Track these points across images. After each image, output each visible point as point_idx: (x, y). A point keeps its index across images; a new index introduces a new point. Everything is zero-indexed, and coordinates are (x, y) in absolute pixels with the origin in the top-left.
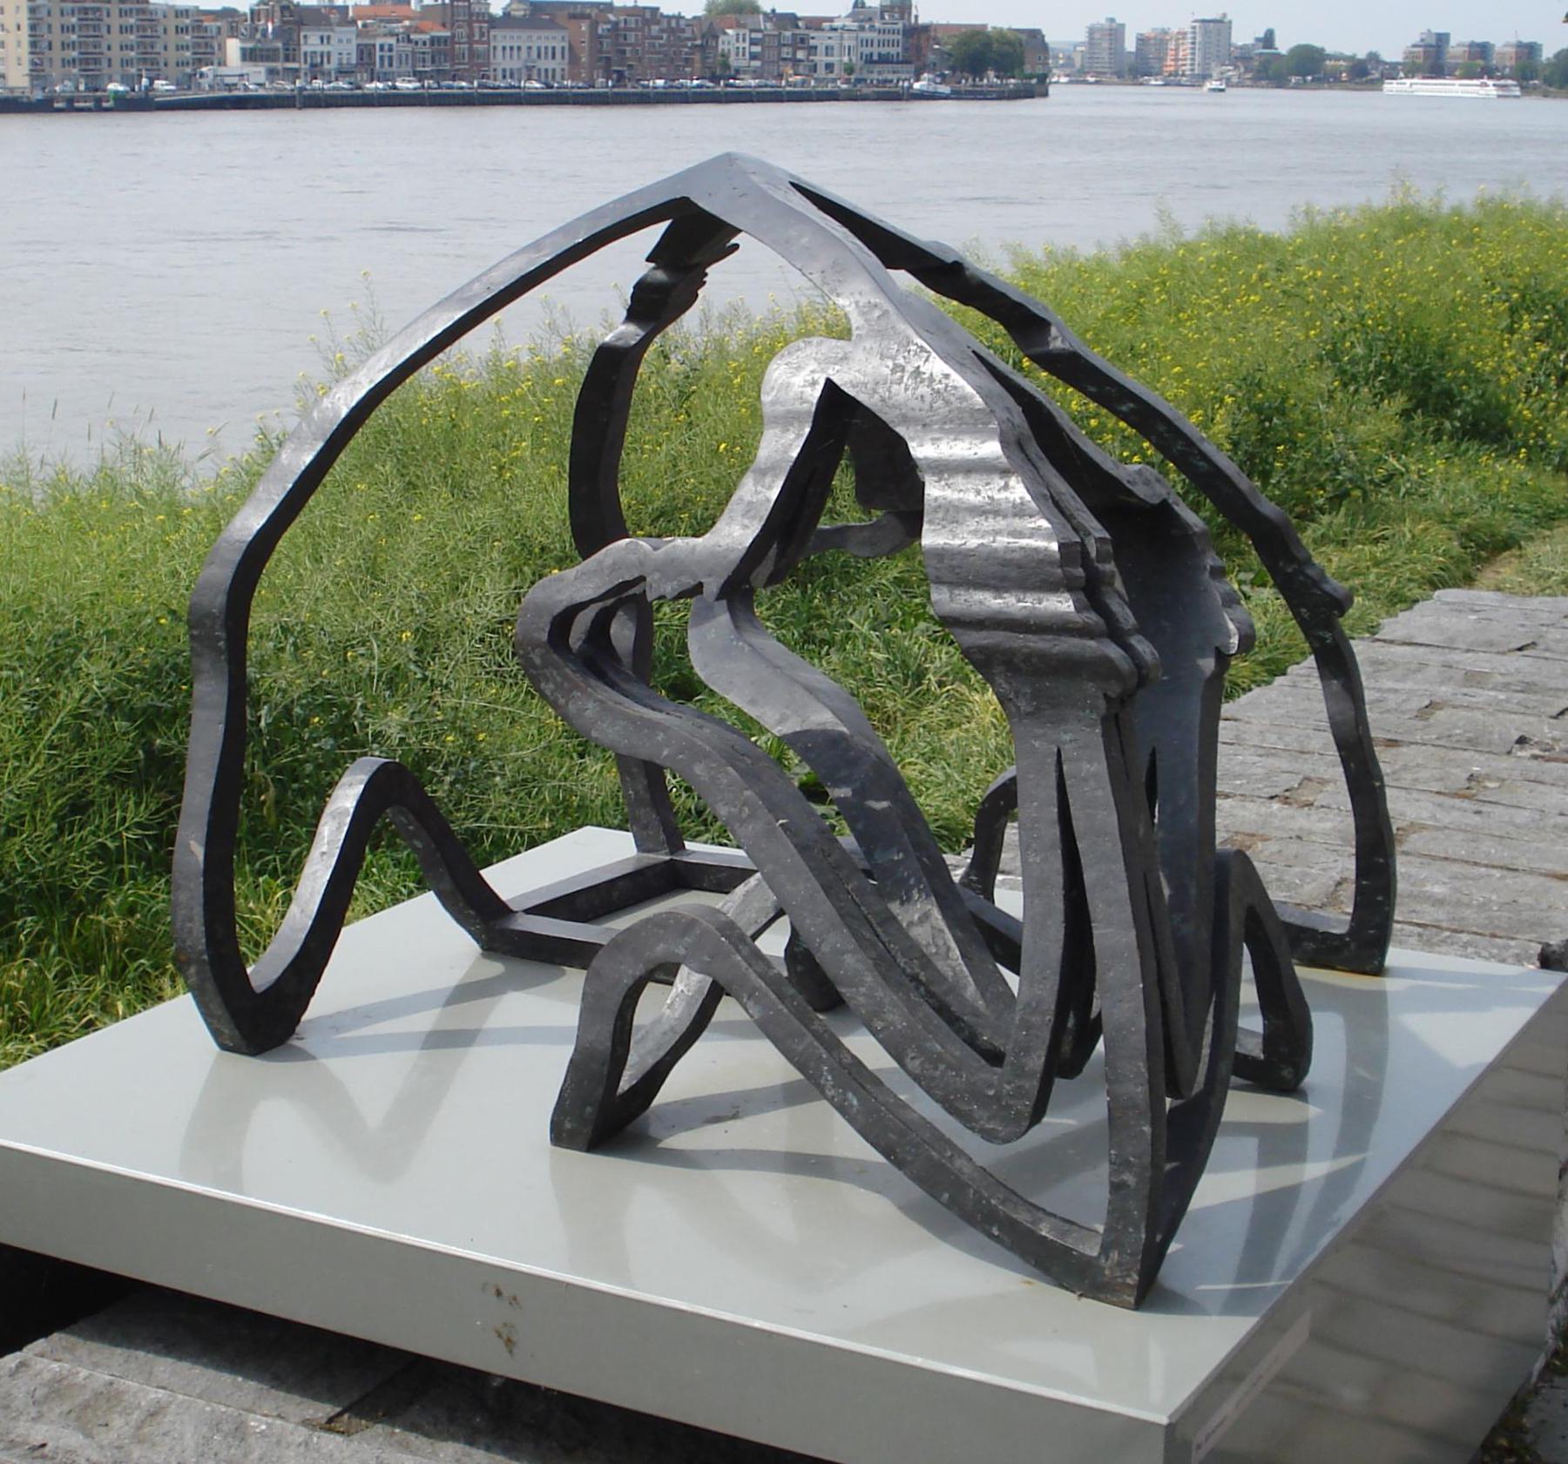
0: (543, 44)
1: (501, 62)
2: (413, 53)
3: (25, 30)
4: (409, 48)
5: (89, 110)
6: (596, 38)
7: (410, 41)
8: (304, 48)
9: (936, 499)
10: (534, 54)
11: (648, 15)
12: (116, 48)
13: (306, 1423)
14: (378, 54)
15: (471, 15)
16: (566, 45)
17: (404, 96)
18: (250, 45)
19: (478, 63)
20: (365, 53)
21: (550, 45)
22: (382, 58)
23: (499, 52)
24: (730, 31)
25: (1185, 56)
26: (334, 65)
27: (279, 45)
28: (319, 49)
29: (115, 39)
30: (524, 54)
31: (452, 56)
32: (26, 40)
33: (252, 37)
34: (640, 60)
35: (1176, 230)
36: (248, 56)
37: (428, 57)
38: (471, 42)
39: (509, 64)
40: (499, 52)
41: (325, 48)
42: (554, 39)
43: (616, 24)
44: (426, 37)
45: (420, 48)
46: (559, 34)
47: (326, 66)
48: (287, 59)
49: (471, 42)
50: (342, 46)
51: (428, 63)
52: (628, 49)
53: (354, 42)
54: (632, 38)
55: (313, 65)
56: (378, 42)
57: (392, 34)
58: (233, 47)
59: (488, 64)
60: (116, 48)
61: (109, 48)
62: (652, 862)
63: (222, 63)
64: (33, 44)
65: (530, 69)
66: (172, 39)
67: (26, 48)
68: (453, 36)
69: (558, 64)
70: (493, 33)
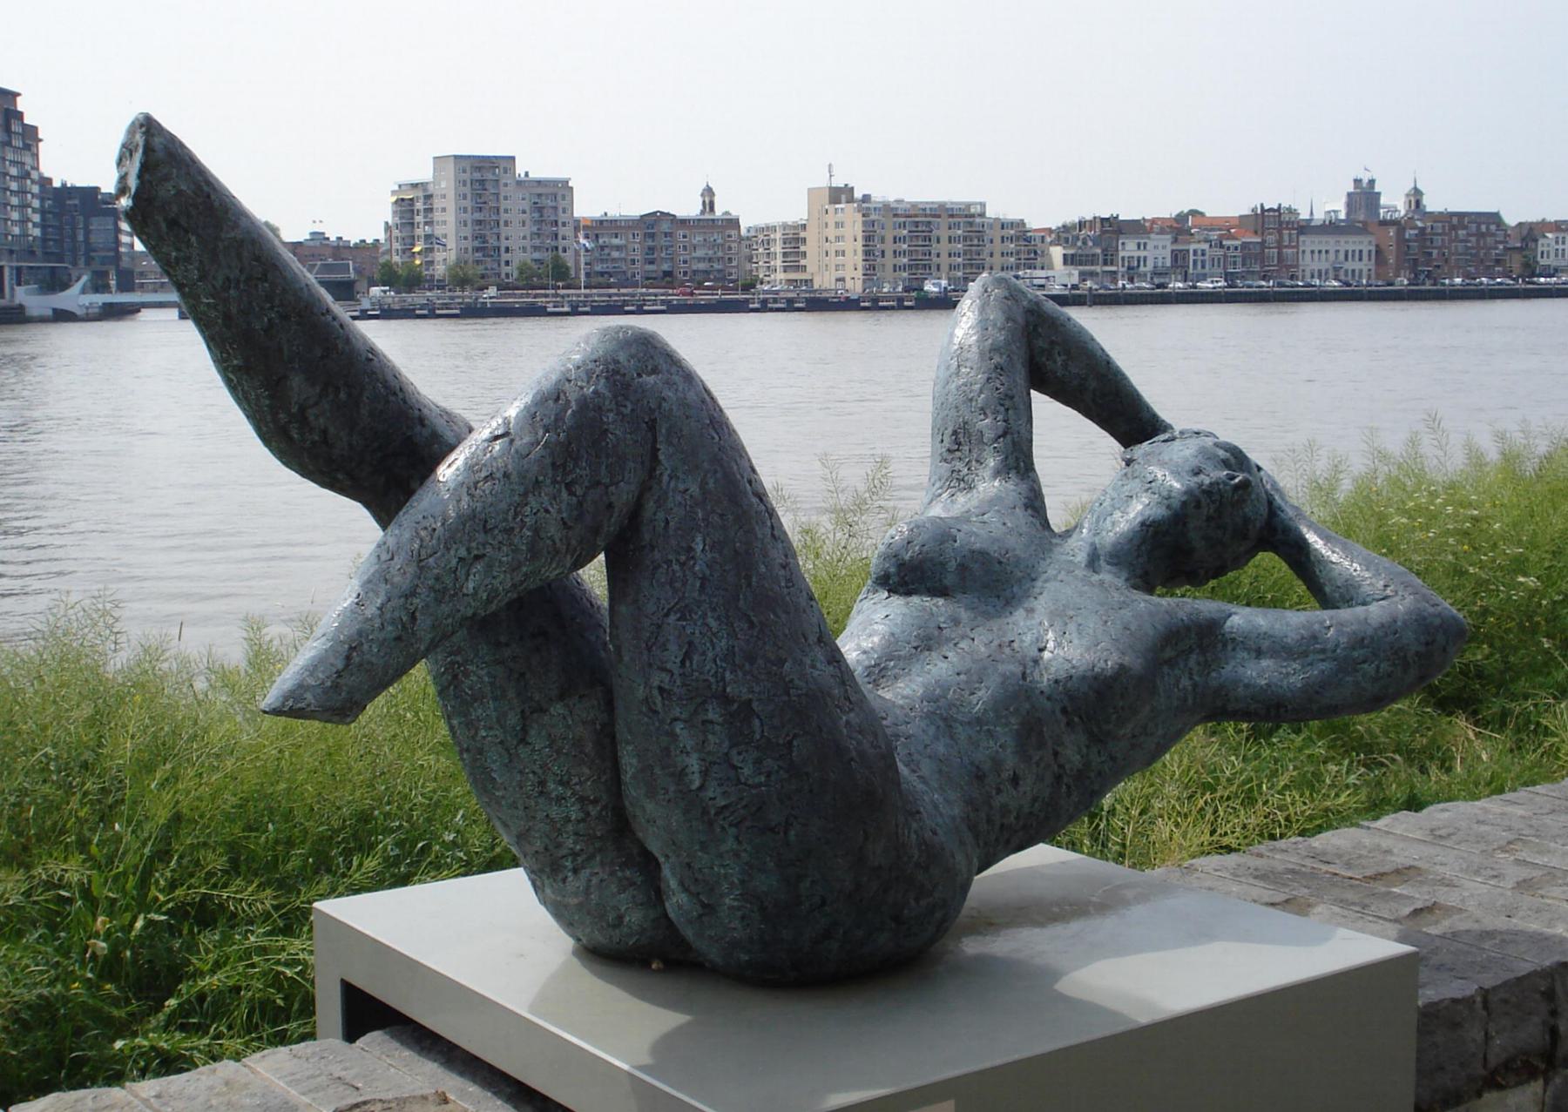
0: (1350, 248)
1: (1309, 264)
2: (1225, 256)
3: (860, 242)
4: (1220, 252)
5: (892, 308)
6: (1401, 240)
7: (1222, 246)
8: (1121, 254)
9: (942, 712)
10: (1342, 256)
11: (1455, 221)
12: (944, 255)
13: (1449, 911)
14: (1192, 258)
15: (1281, 223)
16: (1373, 248)
17: (1203, 294)
18: (1071, 251)
19: (1288, 267)
20: (1179, 258)
21: (1357, 248)
22: (1195, 262)
23: (1308, 255)
24: (1550, 235)
25: (838, 264)
26: (1150, 266)
27: (1099, 251)
28: (1136, 254)
29: (944, 247)
30: (1332, 256)
31: (1261, 258)
32: (860, 249)
33: (1074, 244)
34: (1446, 261)
35: (1384, 456)
36: (1067, 260)
37: (1239, 260)
38: (1280, 247)
39: (1316, 266)
40: (1308, 255)
41: (1142, 254)
42: (1364, 244)
43: (1422, 230)
44: (1237, 243)
45: (1231, 253)
46: (1365, 239)
47: (1142, 268)
48: (1105, 263)
49: (1280, 247)
50: (1159, 251)
51: (1239, 265)
52: (1435, 252)
53: (1169, 248)
54: (1438, 240)
55: (1129, 268)
56: (1192, 247)
57: (1206, 241)
58: (1057, 253)
59: (1297, 266)
60: (944, 255)
61: (991, 255)
62: (1063, 859)
63: (1051, 267)
64: (867, 253)
65: (1336, 270)
66: (998, 247)
67: (860, 256)
68: (1264, 242)
69: (1365, 265)
70: (1302, 238)
